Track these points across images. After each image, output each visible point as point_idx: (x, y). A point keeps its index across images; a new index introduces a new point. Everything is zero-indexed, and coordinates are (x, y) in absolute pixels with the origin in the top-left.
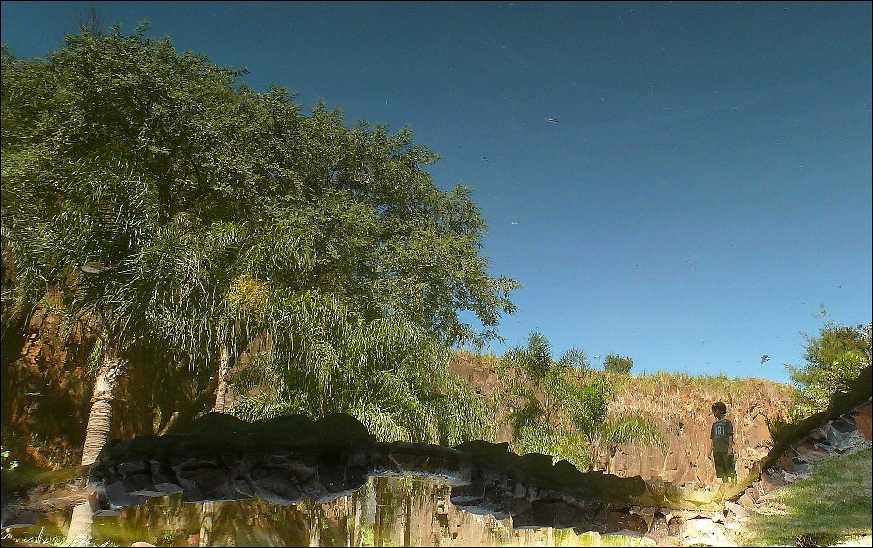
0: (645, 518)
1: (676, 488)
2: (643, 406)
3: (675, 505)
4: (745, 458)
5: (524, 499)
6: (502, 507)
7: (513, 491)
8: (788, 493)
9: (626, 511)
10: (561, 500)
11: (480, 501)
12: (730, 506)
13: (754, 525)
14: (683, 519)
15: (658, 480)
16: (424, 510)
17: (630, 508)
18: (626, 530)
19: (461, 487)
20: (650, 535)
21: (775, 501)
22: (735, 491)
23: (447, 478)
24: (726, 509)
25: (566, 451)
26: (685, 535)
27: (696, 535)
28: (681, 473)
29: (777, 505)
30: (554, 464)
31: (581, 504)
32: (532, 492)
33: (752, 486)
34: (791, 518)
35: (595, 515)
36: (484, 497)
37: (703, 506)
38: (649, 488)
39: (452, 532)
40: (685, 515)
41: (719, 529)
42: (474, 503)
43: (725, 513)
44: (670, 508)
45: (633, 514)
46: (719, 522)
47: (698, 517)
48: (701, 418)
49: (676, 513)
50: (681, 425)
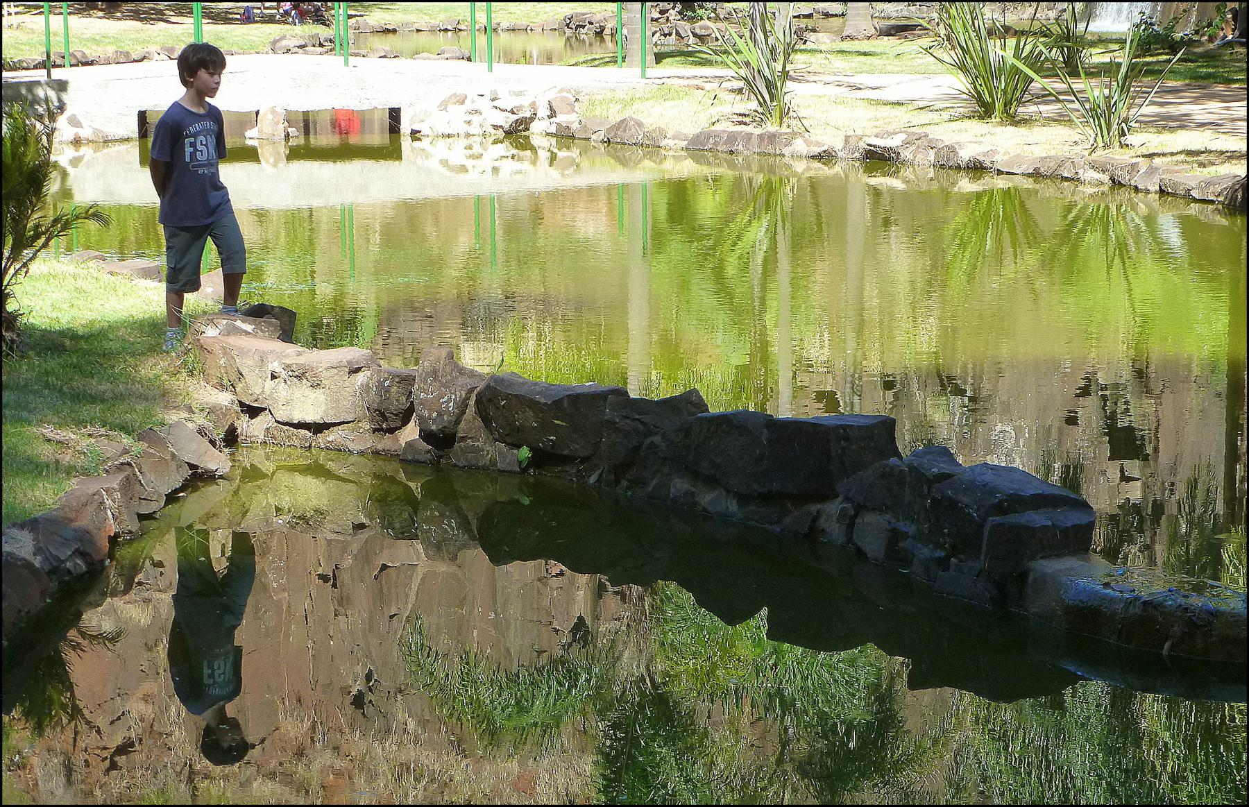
0: (483, 434)
1: (382, 518)
2: (478, 772)
3: (390, 468)
4: (159, 595)
5: (859, 509)
6: (929, 489)
7: (895, 536)
8: (30, 493)
9: (541, 458)
10: (743, 499)
11: (999, 509)
12: (217, 461)
13: (144, 398)
14: (366, 425)
15: (437, 548)
16: (1184, 474)
17: (528, 466)
18: (543, 400)
19: (1060, 555)
20: (470, 382)
21: (70, 471)
22: (193, 507)
23: (1106, 585)
24: (227, 450)
25: (727, 648)
26: (361, 378)
27: (325, 374)
28: (365, 556)
29: (67, 458)
30: (764, 612)
31: (680, 485)
32: (833, 529)
33: (142, 517)
34: (25, 414)
35: (636, 449)
36: (985, 521)
37: (302, 462)
38: (465, 525)
39: (1092, 402)
40: (358, 438)
41: (257, 387)
42: (1017, 502)
43: (231, 438)
44: (407, 460)
45: (518, 447)
46: (253, 412)
47: (318, 428)
48: (293, 728)
49: (385, 442)
50: (358, 702)
